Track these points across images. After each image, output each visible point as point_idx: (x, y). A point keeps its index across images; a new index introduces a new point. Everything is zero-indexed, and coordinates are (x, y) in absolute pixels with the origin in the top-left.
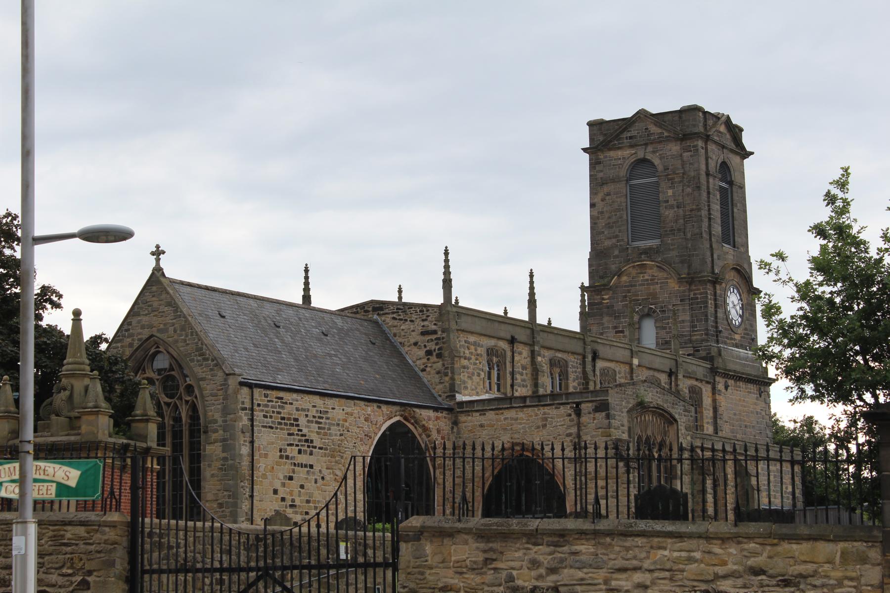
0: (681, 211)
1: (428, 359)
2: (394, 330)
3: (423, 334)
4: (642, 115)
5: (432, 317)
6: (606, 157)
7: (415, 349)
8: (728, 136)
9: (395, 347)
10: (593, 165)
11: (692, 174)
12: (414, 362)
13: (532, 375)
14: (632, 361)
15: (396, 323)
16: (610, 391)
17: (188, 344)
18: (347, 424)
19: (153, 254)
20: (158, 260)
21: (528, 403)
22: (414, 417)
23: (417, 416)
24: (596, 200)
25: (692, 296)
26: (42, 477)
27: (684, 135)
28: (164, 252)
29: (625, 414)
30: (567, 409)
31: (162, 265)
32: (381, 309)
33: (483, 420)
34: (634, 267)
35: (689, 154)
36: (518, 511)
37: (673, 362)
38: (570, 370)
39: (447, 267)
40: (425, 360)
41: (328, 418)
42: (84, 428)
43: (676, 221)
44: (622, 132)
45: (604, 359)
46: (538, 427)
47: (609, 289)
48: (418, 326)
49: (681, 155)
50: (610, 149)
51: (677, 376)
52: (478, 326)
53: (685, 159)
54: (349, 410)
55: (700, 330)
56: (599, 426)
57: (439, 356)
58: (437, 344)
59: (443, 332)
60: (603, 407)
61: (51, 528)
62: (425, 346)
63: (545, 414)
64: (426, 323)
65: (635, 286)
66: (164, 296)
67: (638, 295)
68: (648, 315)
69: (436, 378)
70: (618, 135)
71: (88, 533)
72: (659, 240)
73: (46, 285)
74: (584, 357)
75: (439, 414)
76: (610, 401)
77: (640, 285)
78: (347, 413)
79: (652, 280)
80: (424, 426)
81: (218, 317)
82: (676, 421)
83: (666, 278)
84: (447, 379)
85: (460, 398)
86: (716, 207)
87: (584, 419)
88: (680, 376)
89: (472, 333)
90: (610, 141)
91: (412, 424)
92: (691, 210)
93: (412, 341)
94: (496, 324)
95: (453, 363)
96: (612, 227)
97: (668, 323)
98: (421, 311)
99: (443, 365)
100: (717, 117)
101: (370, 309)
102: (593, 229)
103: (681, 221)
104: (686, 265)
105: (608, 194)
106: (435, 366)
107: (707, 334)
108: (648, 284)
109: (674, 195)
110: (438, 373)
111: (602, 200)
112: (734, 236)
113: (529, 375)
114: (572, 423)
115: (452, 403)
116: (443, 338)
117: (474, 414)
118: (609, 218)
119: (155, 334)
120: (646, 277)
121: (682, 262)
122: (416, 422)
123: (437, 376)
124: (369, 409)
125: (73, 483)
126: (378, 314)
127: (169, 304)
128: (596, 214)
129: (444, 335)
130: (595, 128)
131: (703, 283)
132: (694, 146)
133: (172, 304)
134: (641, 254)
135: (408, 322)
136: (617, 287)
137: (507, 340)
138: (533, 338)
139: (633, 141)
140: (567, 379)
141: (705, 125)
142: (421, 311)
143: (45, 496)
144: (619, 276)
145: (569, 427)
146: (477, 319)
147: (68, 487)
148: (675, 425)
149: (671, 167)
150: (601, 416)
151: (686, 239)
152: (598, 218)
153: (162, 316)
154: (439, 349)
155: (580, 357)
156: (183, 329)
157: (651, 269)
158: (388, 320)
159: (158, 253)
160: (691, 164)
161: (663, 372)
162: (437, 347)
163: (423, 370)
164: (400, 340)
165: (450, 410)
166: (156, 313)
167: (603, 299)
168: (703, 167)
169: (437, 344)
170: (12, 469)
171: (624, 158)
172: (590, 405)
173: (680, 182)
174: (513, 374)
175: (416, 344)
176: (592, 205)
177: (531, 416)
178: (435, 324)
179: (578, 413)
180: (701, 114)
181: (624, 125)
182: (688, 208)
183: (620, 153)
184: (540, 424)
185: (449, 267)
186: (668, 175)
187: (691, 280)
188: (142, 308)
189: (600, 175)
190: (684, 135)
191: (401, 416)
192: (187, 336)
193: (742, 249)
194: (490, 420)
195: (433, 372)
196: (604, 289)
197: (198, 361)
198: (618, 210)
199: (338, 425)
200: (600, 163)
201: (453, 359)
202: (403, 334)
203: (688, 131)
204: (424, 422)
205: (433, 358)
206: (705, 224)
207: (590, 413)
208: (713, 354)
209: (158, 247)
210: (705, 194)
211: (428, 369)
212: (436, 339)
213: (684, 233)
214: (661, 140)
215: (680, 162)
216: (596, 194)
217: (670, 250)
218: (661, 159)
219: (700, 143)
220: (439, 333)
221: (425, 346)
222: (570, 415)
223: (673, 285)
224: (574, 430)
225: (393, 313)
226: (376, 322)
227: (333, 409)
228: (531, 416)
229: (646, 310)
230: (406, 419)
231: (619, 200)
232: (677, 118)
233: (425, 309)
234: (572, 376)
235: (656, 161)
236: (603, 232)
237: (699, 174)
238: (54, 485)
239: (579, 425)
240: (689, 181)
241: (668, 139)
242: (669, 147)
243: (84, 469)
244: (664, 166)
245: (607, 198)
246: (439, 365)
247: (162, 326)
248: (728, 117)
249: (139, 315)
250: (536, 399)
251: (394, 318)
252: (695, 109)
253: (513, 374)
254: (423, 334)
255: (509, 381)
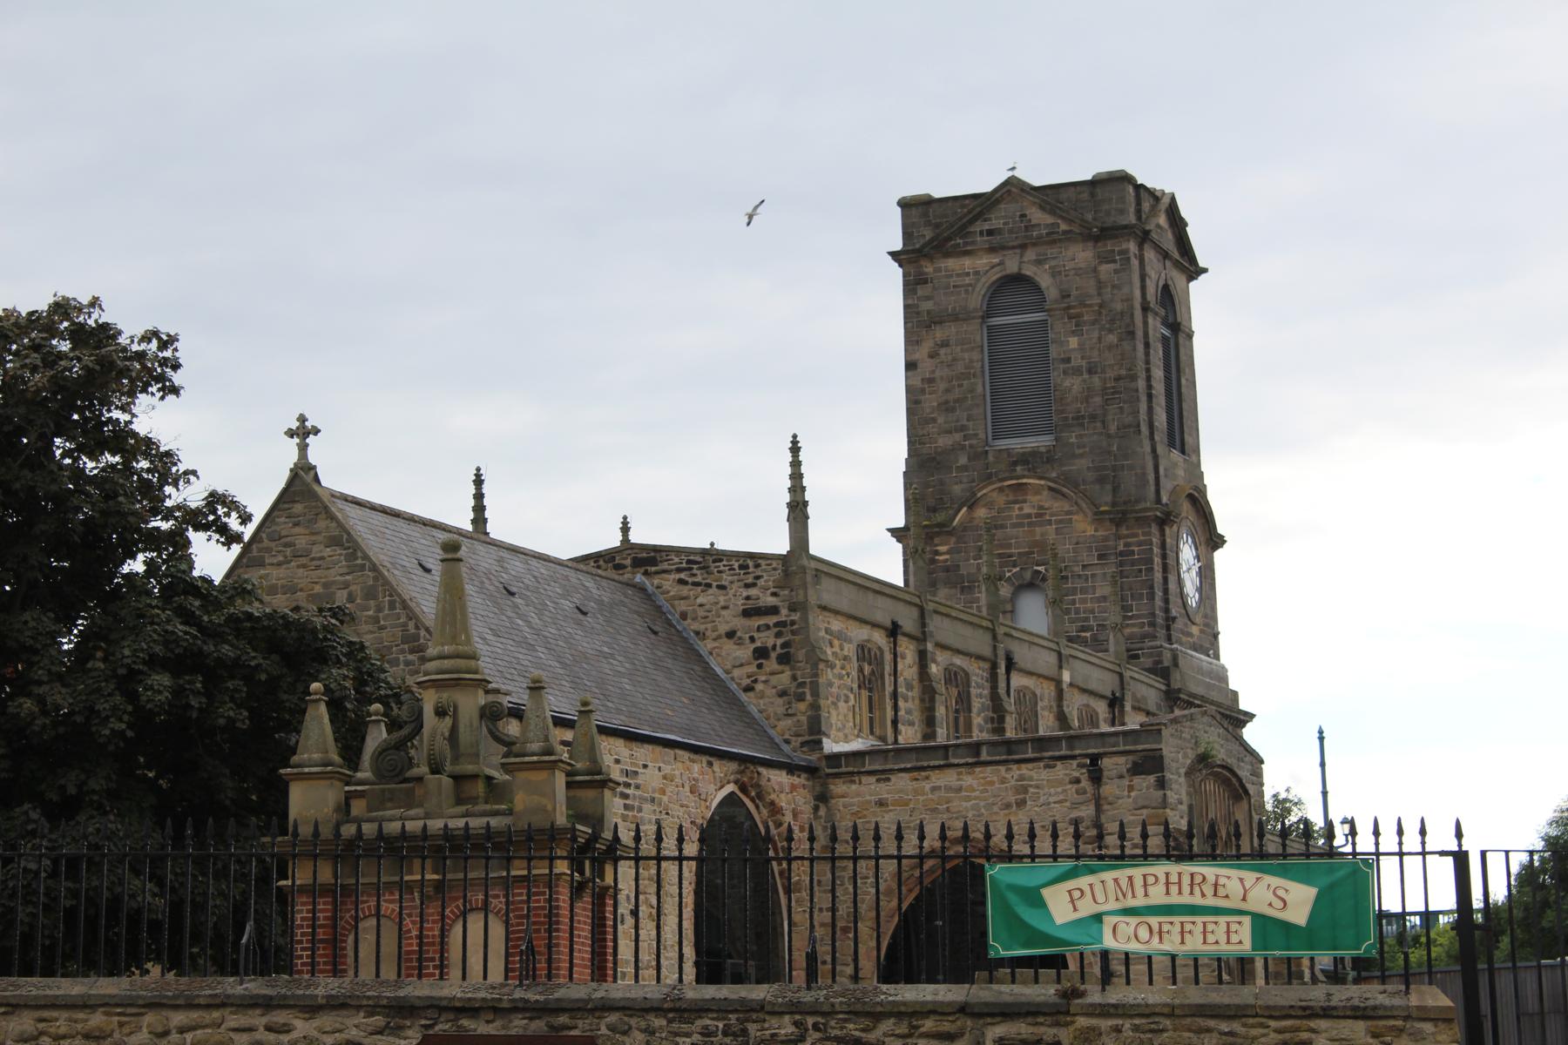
0: (1096, 380)
1: (760, 666)
2: (682, 606)
3: (747, 613)
4: (1012, 188)
5: (768, 579)
6: (938, 270)
7: (729, 646)
8: (1170, 235)
9: (685, 640)
10: (910, 287)
11: (1119, 307)
12: (727, 672)
13: (922, 700)
14: (1060, 675)
15: (685, 590)
16: (1165, 733)
17: (382, 628)
18: (665, 799)
19: (291, 434)
20: (303, 448)
21: (984, 756)
22: (758, 786)
23: (763, 782)
24: (917, 356)
25: (1121, 548)
26: (1210, 901)
27: (1102, 230)
28: (316, 431)
29: (1182, 779)
30: (1071, 769)
31: (313, 458)
32: (652, 561)
33: (883, 790)
34: (1001, 489)
35: (1112, 266)
36: (911, 979)
37: (1116, 677)
38: (973, 691)
39: (796, 476)
40: (752, 668)
41: (637, 787)
42: (520, 800)
43: (1087, 400)
44: (972, 222)
45: (1021, 670)
46: (1008, 806)
47: (950, 533)
48: (737, 597)
49: (1095, 270)
50: (947, 255)
51: (1122, 706)
52: (843, 598)
53: (1103, 277)
54: (667, 769)
55: (1138, 617)
56: (1141, 803)
57: (785, 659)
58: (778, 635)
59: (792, 609)
60: (1150, 764)
61: (1273, 1023)
62: (752, 639)
63: (1021, 778)
64: (753, 592)
65: (1002, 527)
66: (322, 524)
67: (1009, 546)
68: (1031, 586)
69: (779, 705)
70: (964, 226)
71: (1375, 1036)
72: (1051, 437)
73: (220, 491)
74: (994, 666)
75: (796, 780)
76: (1165, 752)
77: (1015, 526)
78: (665, 777)
79: (1039, 515)
80: (772, 803)
81: (420, 572)
82: (1246, 792)
83: (1069, 513)
84: (802, 706)
85: (831, 746)
86: (1158, 373)
87: (1108, 789)
88: (1128, 708)
89: (837, 612)
90: (949, 239)
91: (753, 800)
92: (1118, 379)
93: (723, 628)
94: (871, 595)
95: (816, 675)
96: (953, 410)
97: (1074, 602)
98: (741, 567)
99: (794, 678)
100: (1155, 196)
101: (628, 562)
102: (910, 412)
103: (1098, 400)
104: (1109, 487)
105: (945, 344)
106: (774, 680)
107: (1152, 624)
108: (1030, 524)
109: (1081, 347)
110: (782, 694)
111: (931, 356)
112: (1182, 432)
113: (917, 701)
114: (1081, 798)
115: (814, 757)
116: (793, 623)
117: (864, 779)
118: (947, 391)
119: (303, 604)
120: (1027, 510)
121: (1101, 480)
122: (760, 796)
123: (780, 701)
124: (696, 767)
125: (1299, 915)
126: (646, 573)
127: (334, 542)
128: (917, 383)
129: (796, 617)
130: (914, 211)
131: (1142, 521)
132: (1120, 253)
133: (345, 541)
134: (1015, 463)
135: (714, 590)
136: (965, 529)
137: (885, 629)
138: (924, 625)
139: (996, 239)
140: (970, 711)
141: (1139, 212)
142: (741, 567)
143: (1224, 947)
144: (970, 507)
145: (1075, 805)
146: (843, 585)
147: (1287, 927)
148: (1245, 802)
149: (1074, 293)
150: (1146, 782)
151: (1109, 436)
152: (923, 391)
153: (318, 567)
154: (784, 646)
155: (987, 666)
156: (370, 594)
157: (1037, 493)
158: (667, 585)
159: (303, 432)
160: (1114, 287)
161: (1103, 697)
162: (779, 642)
163: (749, 689)
164: (695, 626)
165: (811, 771)
166: (303, 560)
167: (937, 553)
168: (1137, 293)
169: (778, 635)
170: (1124, 883)
171: (977, 273)
172: (1121, 760)
173: (1094, 323)
174: (895, 695)
175: (731, 635)
176: (910, 366)
177: (992, 783)
178: (774, 594)
179: (1096, 777)
180: (1131, 189)
181: (977, 206)
182: (1110, 374)
183: (967, 263)
184: (1012, 799)
185: (801, 476)
186: (1069, 308)
187: (1120, 516)
188: (268, 550)
189: (927, 306)
190: (1102, 230)
191: (736, 782)
192: (379, 609)
193: (1194, 458)
194: (901, 791)
195: (770, 692)
196: (938, 534)
197: (407, 663)
198: (966, 376)
199: (653, 800)
200: (925, 282)
201: (815, 666)
202: (701, 613)
203: (1109, 221)
204: (773, 796)
205: (772, 664)
206: (1143, 407)
207: (1121, 777)
208: (1166, 664)
209: (302, 419)
210: (1140, 347)
211: (759, 687)
212: (777, 625)
213: (1103, 422)
214: (1053, 239)
215: (1092, 282)
216: (918, 342)
217: (1074, 456)
218: (1053, 276)
219: (1132, 247)
220: (784, 612)
221: (752, 639)
222: (1078, 781)
223: (1084, 526)
224: (1087, 812)
225: (679, 570)
226: (642, 589)
227: (645, 766)
228: (992, 783)
229: (1028, 575)
230: (743, 789)
231: (966, 355)
232: (1085, 196)
233: (751, 563)
234: (976, 704)
235: (1045, 281)
236: (934, 420)
237: (1132, 307)
238: (1247, 920)
239: (1098, 802)
240: (1112, 321)
241: (1068, 237)
242: (1070, 253)
243: (1326, 881)
244: (1061, 291)
245: (942, 351)
246: (784, 679)
247: (318, 589)
248: (1173, 199)
249: (262, 565)
250: (1003, 749)
251: (681, 582)
252: (1123, 178)
253: (895, 695)
254: (747, 613)
255: (889, 714)
